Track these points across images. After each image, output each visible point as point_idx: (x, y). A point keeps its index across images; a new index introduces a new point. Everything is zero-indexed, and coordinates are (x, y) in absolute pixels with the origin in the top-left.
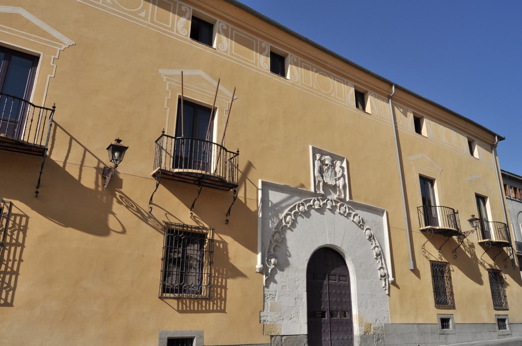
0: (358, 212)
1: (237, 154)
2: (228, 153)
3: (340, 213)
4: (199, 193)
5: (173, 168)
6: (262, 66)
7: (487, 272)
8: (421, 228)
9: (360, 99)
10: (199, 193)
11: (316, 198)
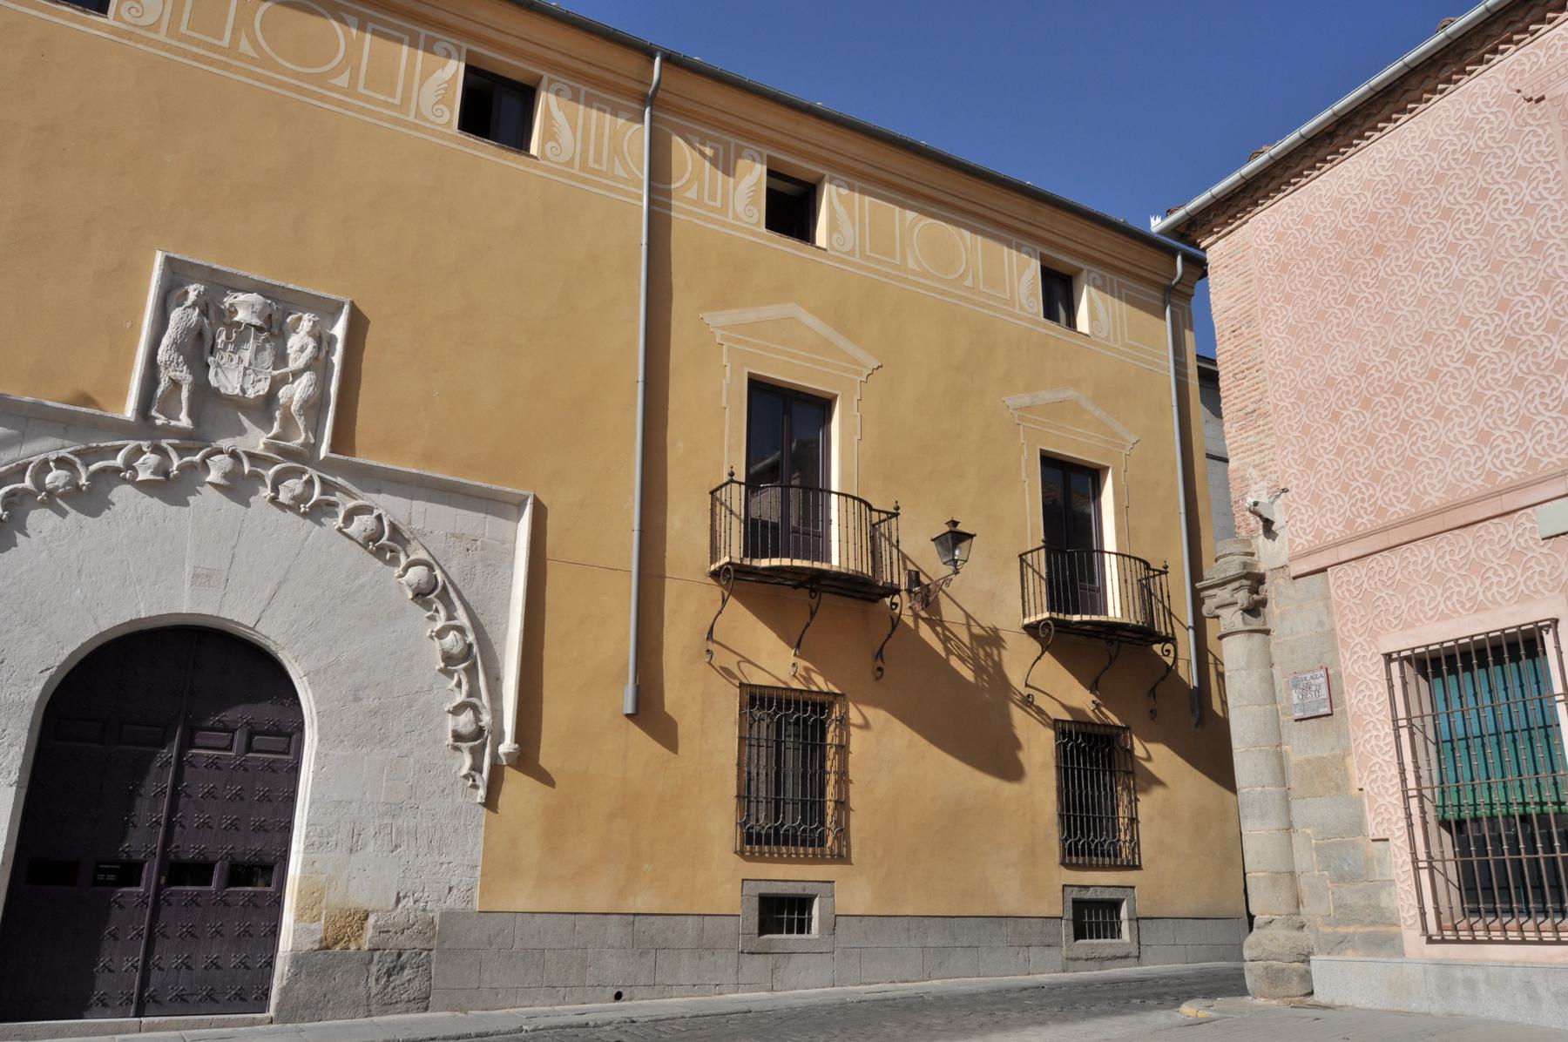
0: (366, 499)
1: (896, 515)
2: (875, 514)
3: (274, 500)
4: (813, 614)
5: (746, 555)
6: (742, 216)
7: (1051, 733)
8: (1027, 621)
9: (1058, 293)
10: (813, 614)
11: (145, 444)
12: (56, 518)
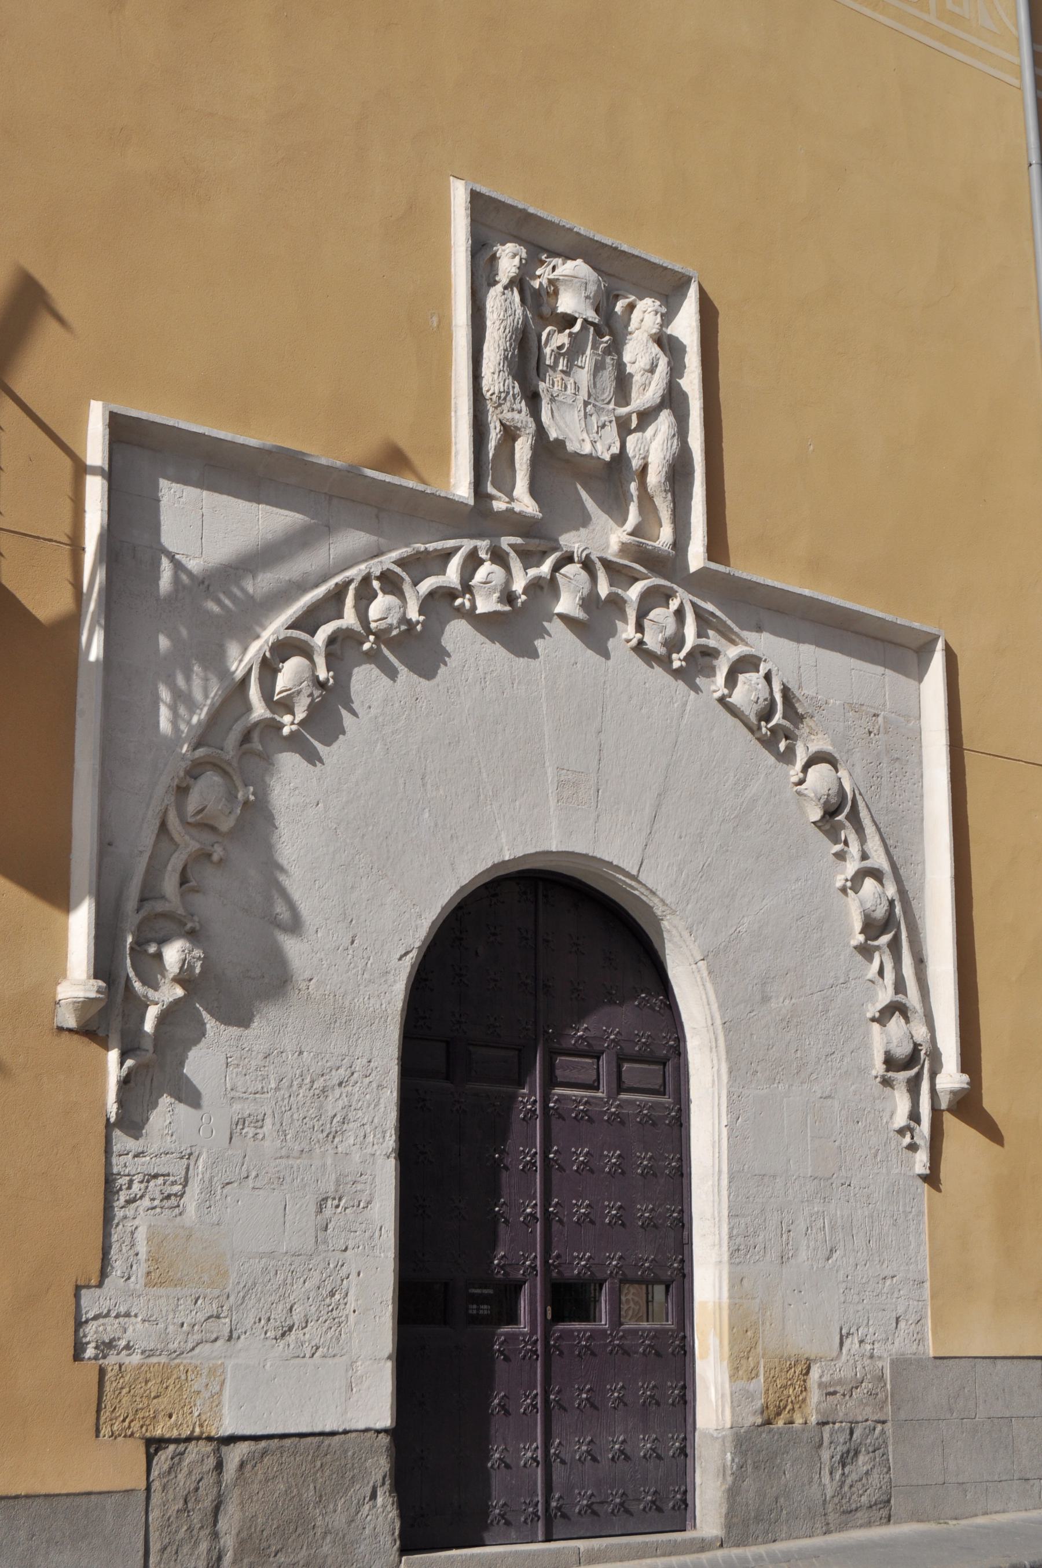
11: (483, 545)
12: (385, 680)
